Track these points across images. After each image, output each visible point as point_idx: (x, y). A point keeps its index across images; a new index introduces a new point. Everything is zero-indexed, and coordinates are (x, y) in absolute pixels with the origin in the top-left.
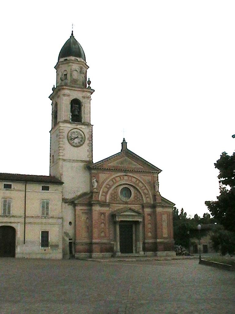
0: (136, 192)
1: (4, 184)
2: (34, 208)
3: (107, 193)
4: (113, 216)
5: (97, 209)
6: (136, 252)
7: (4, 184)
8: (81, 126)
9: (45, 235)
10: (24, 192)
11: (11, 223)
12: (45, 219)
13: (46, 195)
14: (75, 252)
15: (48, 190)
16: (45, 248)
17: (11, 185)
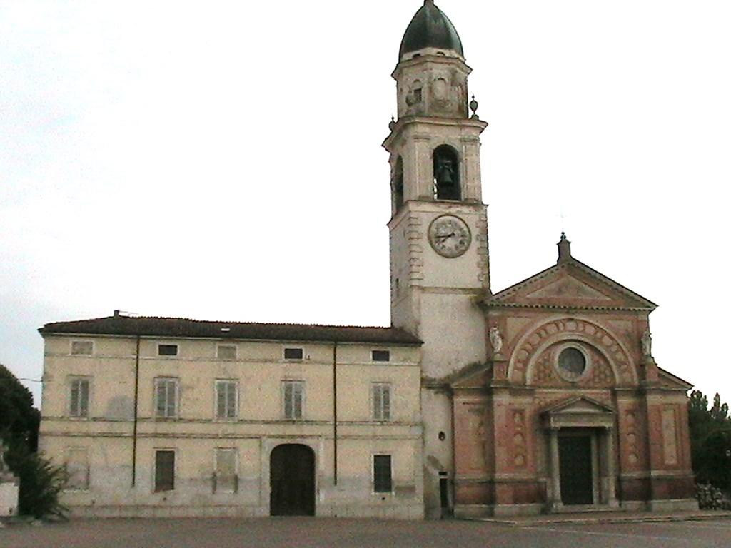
0: (596, 358)
1: (286, 350)
2: (356, 402)
3: (525, 363)
4: (543, 416)
5: (503, 400)
6: (600, 502)
7: (160, 346)
8: (459, 209)
9: (383, 465)
10: (331, 367)
11: (302, 436)
12: (381, 428)
13: (382, 371)
14: (455, 502)
15: (388, 360)
16: (384, 494)
17: (301, 350)
